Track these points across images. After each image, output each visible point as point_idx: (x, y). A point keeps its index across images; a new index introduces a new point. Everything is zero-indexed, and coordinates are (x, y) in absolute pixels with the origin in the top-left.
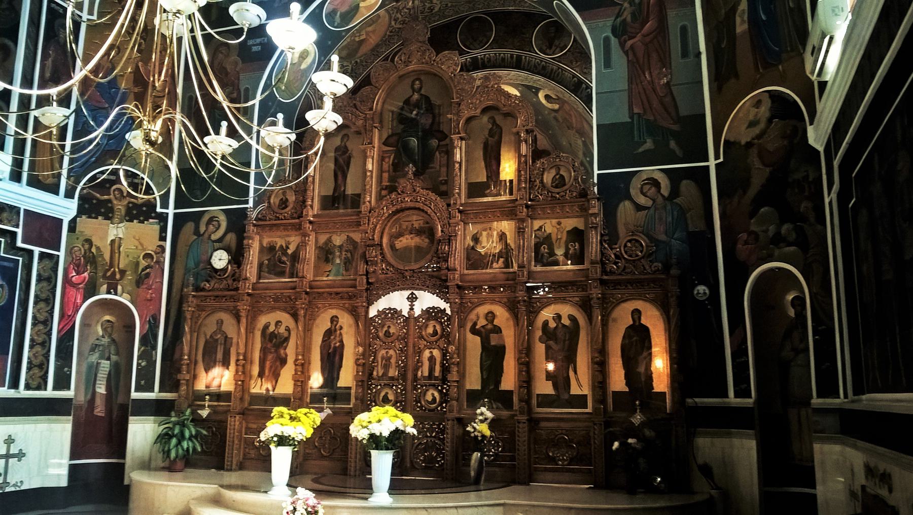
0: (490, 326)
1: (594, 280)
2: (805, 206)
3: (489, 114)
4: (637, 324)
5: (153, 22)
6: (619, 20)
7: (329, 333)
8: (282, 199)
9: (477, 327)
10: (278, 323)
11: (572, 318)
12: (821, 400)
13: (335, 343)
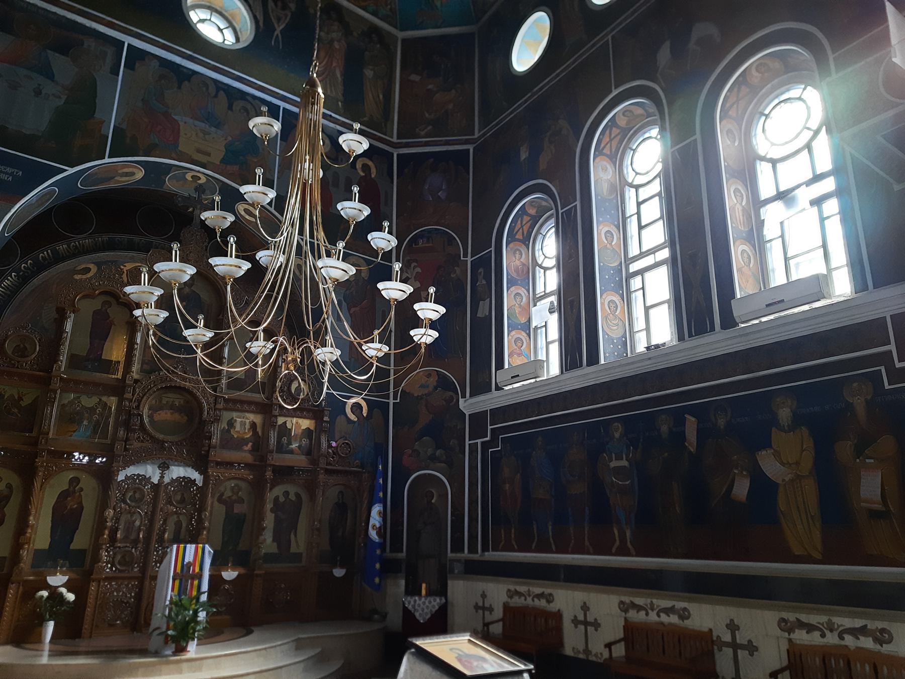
0: (234, 497)
1: (322, 469)
2: (453, 442)
3: (109, 299)
4: (341, 502)
5: (248, 123)
6: (348, 292)
7: (64, 496)
8: (18, 346)
9: (224, 497)
10: (286, 493)
11: (298, 495)
12: (454, 555)
13: (71, 504)
